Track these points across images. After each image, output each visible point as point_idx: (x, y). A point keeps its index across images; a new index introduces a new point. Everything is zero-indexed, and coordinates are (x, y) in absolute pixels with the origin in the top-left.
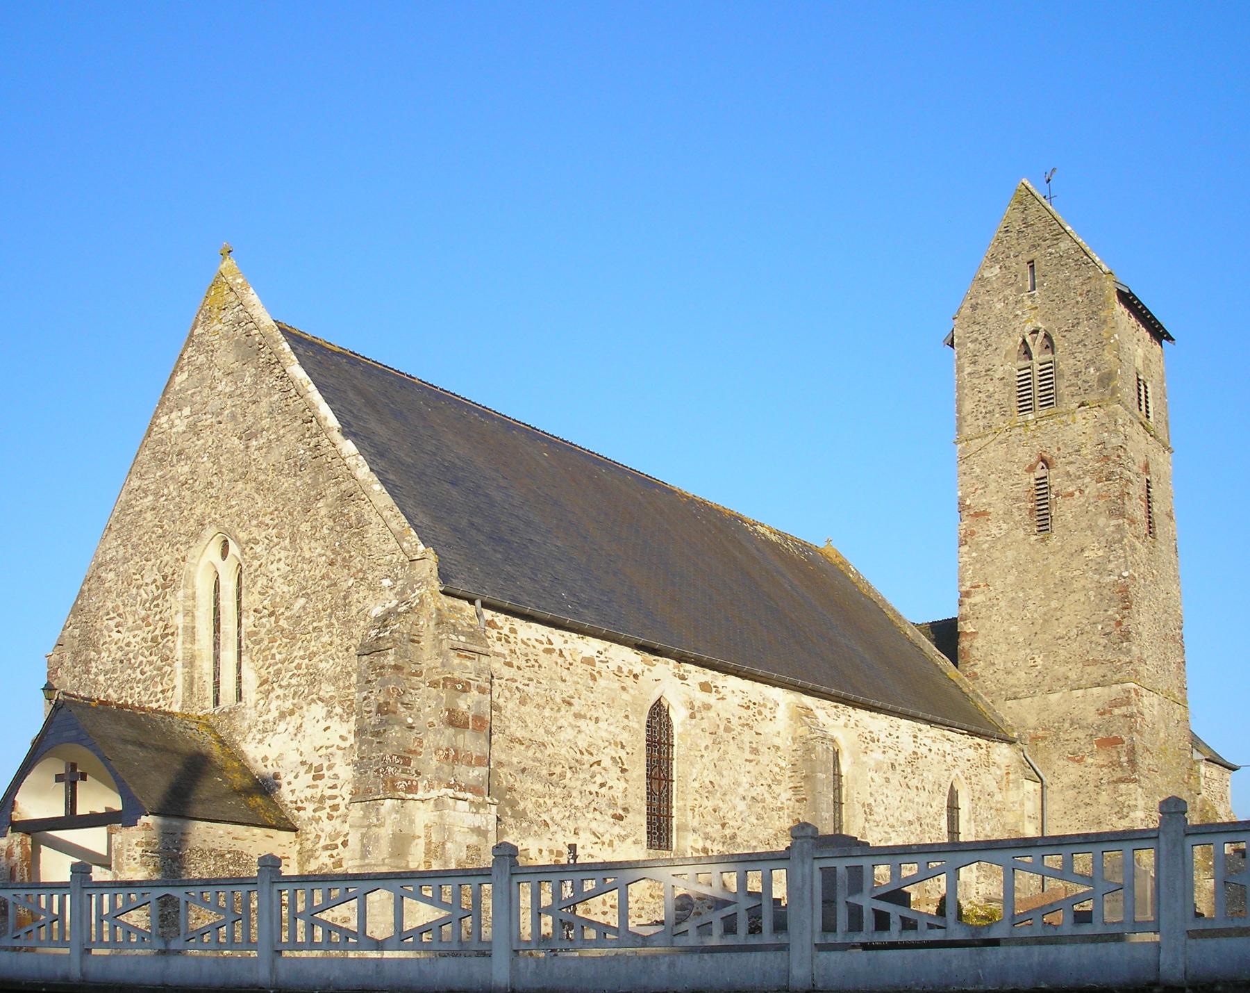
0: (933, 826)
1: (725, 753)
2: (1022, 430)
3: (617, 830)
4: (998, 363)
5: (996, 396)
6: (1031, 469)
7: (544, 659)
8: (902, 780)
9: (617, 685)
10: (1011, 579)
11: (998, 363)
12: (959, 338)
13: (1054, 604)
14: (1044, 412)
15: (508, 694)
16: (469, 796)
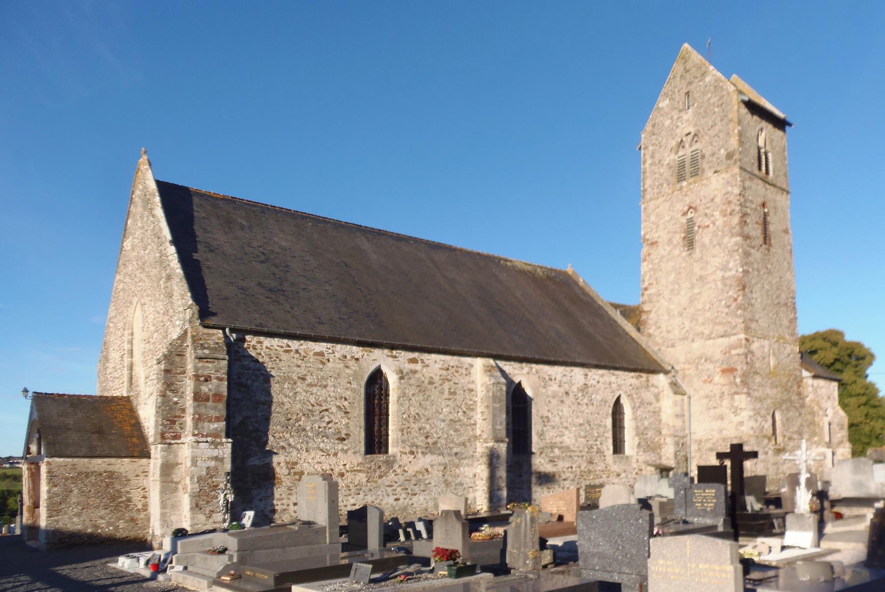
1: (429, 396)
3: (340, 446)
6: (685, 214)
7: (284, 357)
9: (342, 365)
13: (696, 291)
15: (253, 377)
16: (209, 439)
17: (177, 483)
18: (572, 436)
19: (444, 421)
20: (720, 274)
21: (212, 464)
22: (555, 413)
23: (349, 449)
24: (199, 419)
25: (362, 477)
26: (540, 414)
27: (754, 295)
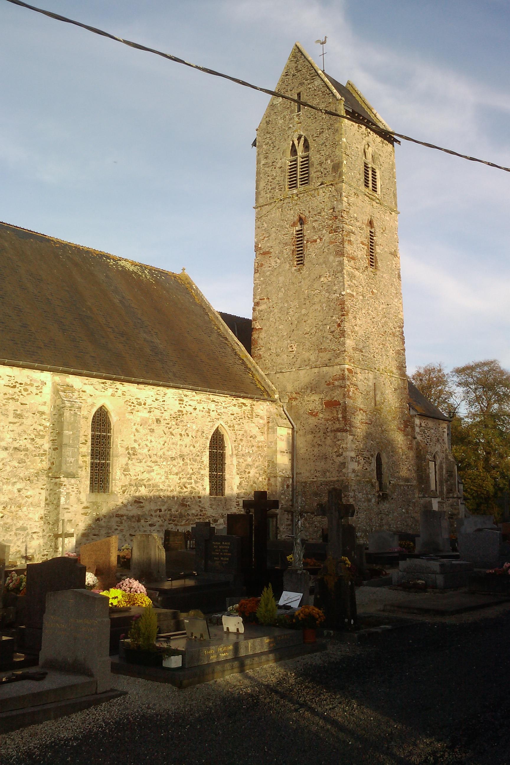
2: (290, 200)
4: (279, 158)
5: (277, 178)
10: (281, 295)
11: (279, 158)
12: (259, 142)
13: (304, 311)
14: (301, 188)
18: (162, 472)
19: (6, 449)
22: (143, 443)
26: (125, 444)
27: (358, 322)
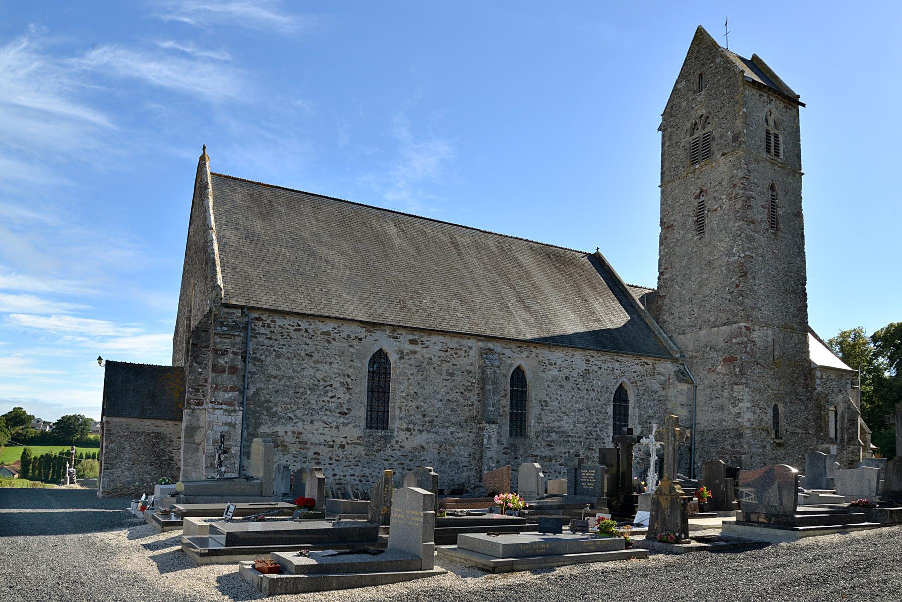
0: (600, 412)
3: (342, 420)
7: (294, 334)
8: (574, 386)
13: (704, 276)
15: (266, 353)
16: (224, 407)
17: (199, 444)
18: (571, 421)
20: (725, 259)
21: (226, 428)
23: (349, 423)
24: (216, 388)
25: (361, 449)
26: (539, 397)
